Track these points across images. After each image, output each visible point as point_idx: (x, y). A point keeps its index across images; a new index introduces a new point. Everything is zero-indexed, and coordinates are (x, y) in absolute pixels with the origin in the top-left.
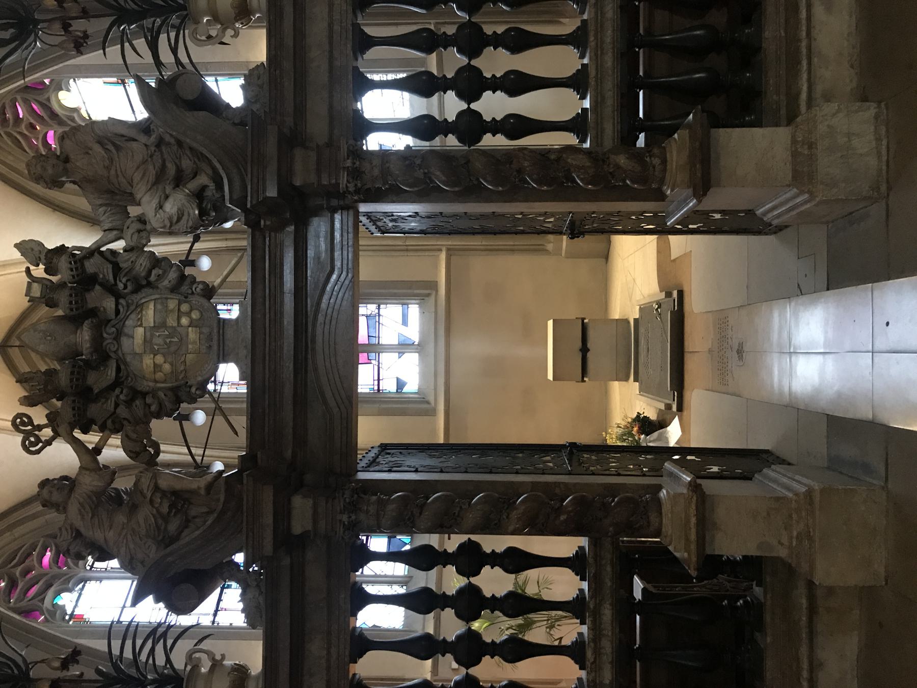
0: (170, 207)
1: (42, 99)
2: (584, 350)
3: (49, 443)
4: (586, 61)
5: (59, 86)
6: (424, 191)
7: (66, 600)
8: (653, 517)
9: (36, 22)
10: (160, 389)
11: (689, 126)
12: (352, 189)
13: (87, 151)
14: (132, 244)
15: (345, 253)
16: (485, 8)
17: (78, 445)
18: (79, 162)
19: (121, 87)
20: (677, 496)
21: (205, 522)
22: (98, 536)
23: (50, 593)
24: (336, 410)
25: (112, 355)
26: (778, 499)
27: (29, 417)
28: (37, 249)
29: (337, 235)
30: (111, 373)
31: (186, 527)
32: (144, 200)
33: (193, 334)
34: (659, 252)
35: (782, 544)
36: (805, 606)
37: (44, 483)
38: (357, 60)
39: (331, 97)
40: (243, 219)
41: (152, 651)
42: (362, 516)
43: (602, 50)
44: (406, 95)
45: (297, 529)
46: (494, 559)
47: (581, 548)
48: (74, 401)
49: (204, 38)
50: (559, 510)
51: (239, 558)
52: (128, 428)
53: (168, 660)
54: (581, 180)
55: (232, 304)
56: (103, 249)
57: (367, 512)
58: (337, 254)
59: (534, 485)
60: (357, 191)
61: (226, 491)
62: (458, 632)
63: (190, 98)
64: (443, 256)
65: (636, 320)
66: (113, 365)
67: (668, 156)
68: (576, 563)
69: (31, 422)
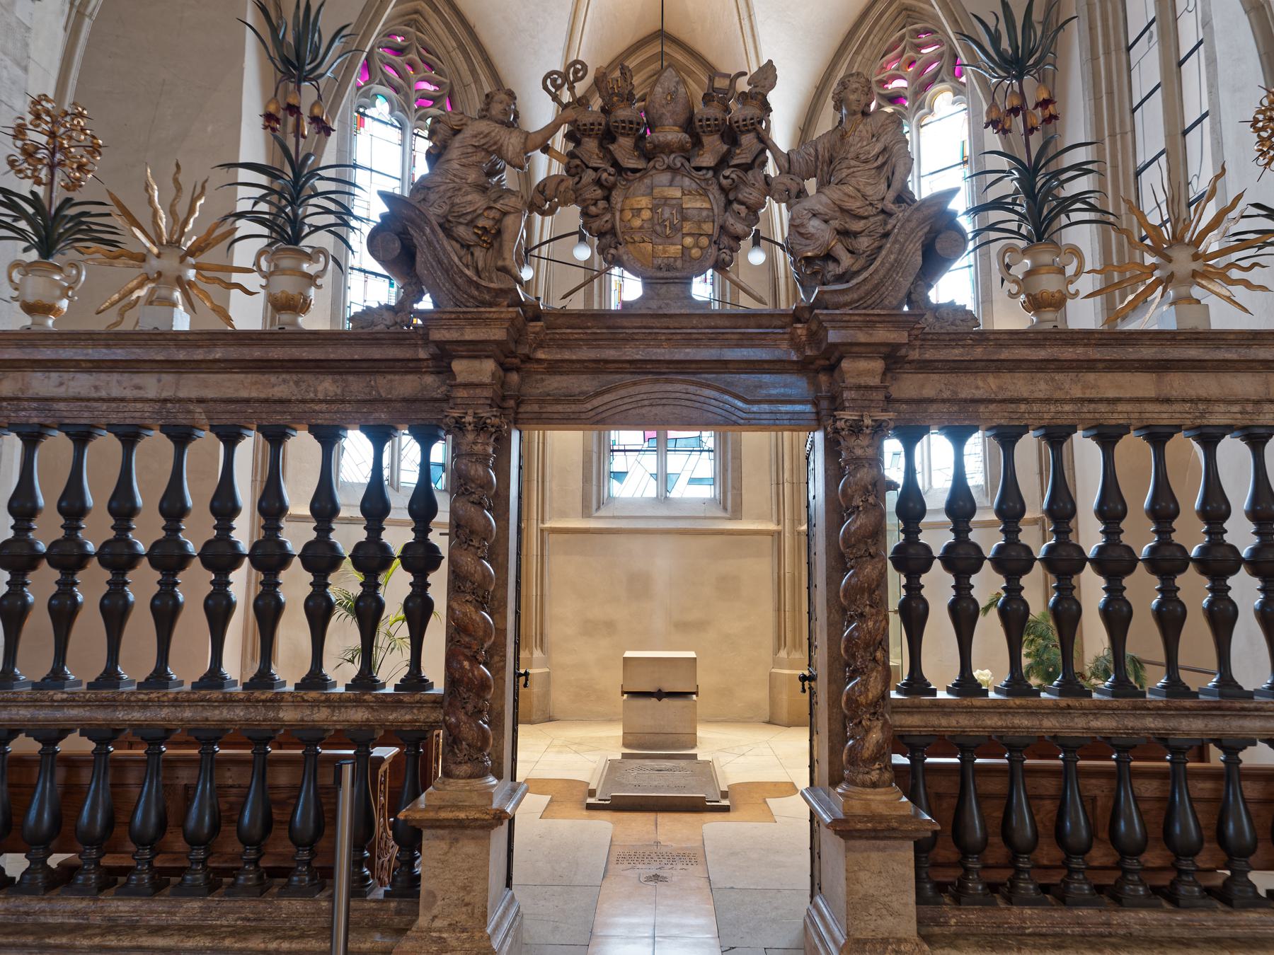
0: (814, 225)
1: (943, 74)
2: (660, 695)
3: (555, 98)
4: (992, 695)
5: (958, 91)
6: (838, 508)
7: (381, 108)
8: (465, 769)
9: (1019, 78)
10: (613, 214)
11: (917, 815)
12: (840, 424)
13: (875, 136)
14: (774, 184)
15: (767, 416)
16: (1051, 577)
17: (552, 129)
18: (864, 128)
19: (960, 160)
20: (490, 796)
21: (467, 266)
22: (454, 153)
23: (389, 91)
24: (589, 406)
25: (651, 164)
26: (484, 915)
27: (582, 78)
28: (767, 83)
29: (789, 408)
30: (632, 163)
31: (462, 246)
32: (824, 199)
33: (675, 250)
34: (775, 784)
35: (433, 920)
36: (362, 946)
37: (511, 95)
38: (988, 430)
39: (944, 401)
40: (803, 304)
41: (328, 211)
42: (470, 437)
43: (1006, 714)
44: (949, 485)
45: (457, 366)
46: (420, 586)
47: (431, 686)
48: (600, 124)
49: (1007, 260)
50: (474, 660)
51: (426, 303)
52: (571, 182)
53: (318, 228)
54: (853, 688)
55: (712, 284)
56: (768, 153)
57: (475, 443)
58: (766, 407)
59: (502, 632)
60: (836, 431)
61: (501, 290)
62: (340, 546)
63: (938, 246)
64: (772, 526)
65: (694, 756)
66: (640, 164)
67: (883, 790)
68: (414, 680)
69: (577, 79)
